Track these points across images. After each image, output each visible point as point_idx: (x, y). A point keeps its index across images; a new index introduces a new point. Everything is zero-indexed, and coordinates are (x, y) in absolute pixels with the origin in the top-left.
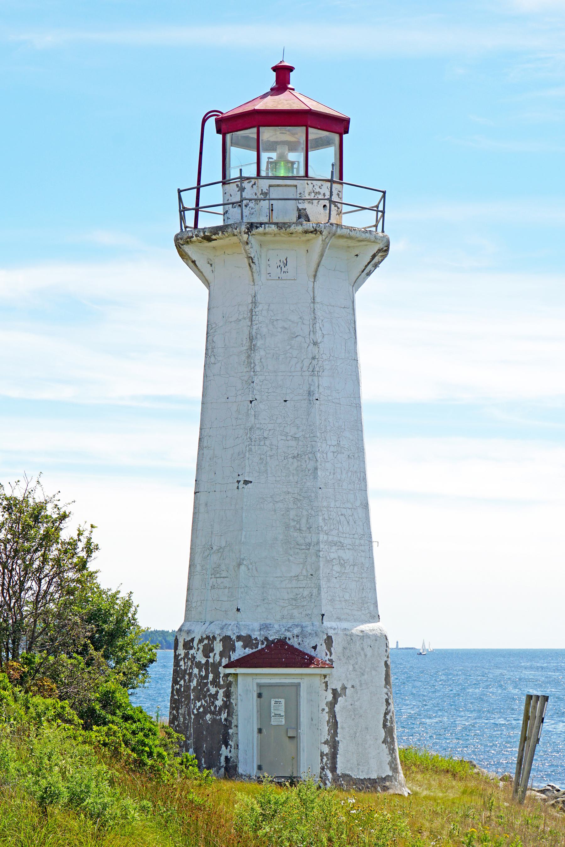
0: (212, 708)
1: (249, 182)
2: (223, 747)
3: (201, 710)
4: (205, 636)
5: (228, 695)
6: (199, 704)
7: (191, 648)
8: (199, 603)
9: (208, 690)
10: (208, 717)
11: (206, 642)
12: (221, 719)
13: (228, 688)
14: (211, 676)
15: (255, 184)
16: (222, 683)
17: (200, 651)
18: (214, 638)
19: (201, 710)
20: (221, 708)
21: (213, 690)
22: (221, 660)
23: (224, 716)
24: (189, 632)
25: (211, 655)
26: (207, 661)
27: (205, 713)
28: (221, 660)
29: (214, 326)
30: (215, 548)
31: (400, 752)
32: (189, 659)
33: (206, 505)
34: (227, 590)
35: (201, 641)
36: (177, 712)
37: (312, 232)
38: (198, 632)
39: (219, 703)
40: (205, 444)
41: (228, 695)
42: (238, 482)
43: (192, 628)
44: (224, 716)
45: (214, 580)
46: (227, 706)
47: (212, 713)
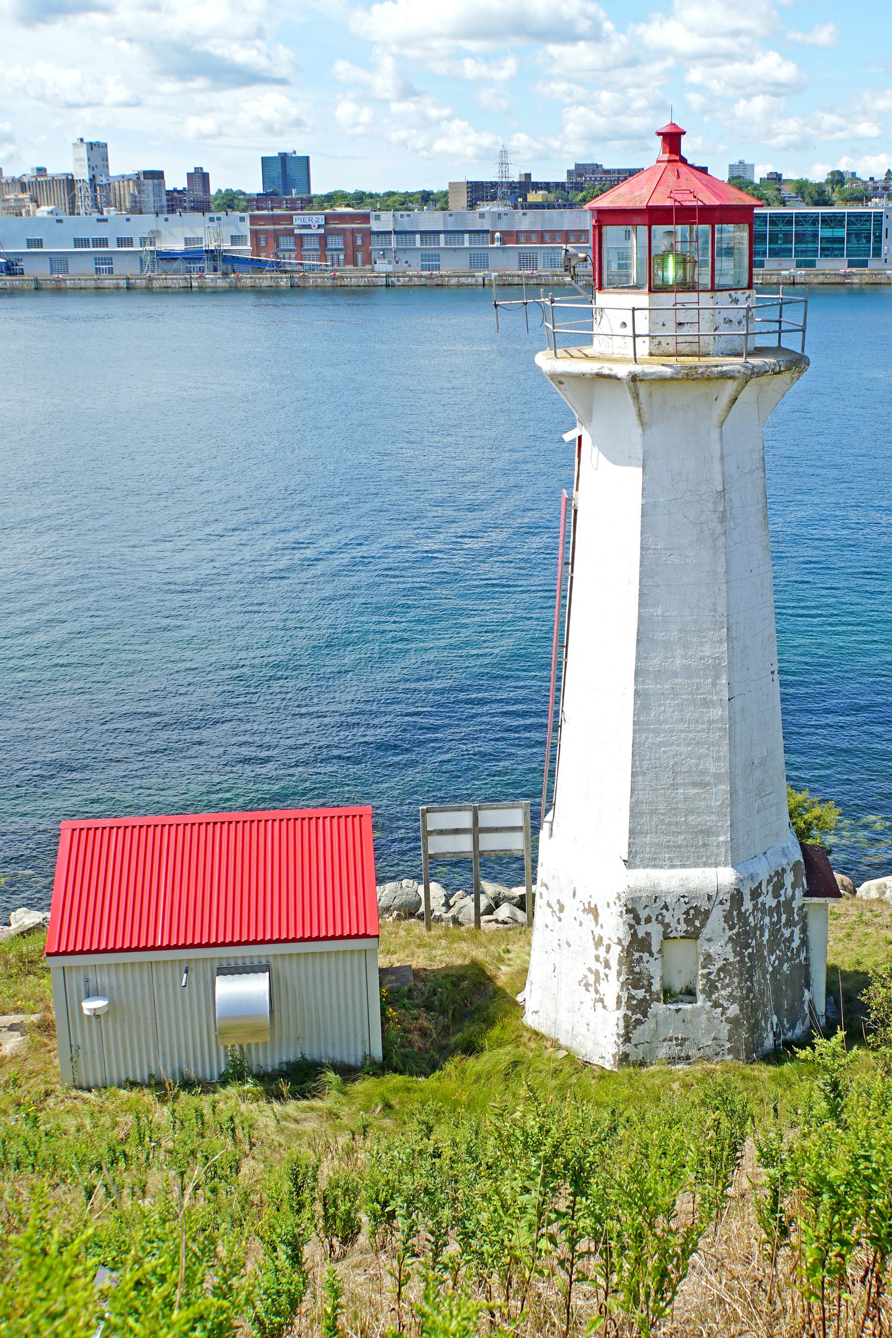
0: (789, 954)
1: (743, 293)
2: (806, 991)
3: (777, 963)
4: (773, 874)
5: (804, 930)
6: (773, 958)
7: (759, 895)
8: (746, 837)
9: (782, 935)
10: (786, 966)
11: (775, 879)
12: (801, 961)
13: (804, 922)
14: (784, 917)
15: (749, 297)
16: (797, 918)
17: (770, 893)
18: (784, 870)
19: (777, 963)
20: (798, 950)
21: (787, 933)
22: (793, 892)
23: (803, 956)
24: (752, 877)
25: (782, 892)
26: (779, 902)
27: (781, 965)
28: (793, 892)
29: (730, 479)
30: (756, 761)
31: (654, 863)
32: (758, 910)
33: (742, 711)
34: (774, 808)
35: (769, 882)
36: (752, 982)
37: (717, 378)
38: (763, 872)
39: (796, 944)
40: (734, 634)
41: (804, 930)
42: (773, 672)
43: (751, 870)
44: (803, 956)
45: (759, 801)
46: (804, 942)
47: (790, 960)
